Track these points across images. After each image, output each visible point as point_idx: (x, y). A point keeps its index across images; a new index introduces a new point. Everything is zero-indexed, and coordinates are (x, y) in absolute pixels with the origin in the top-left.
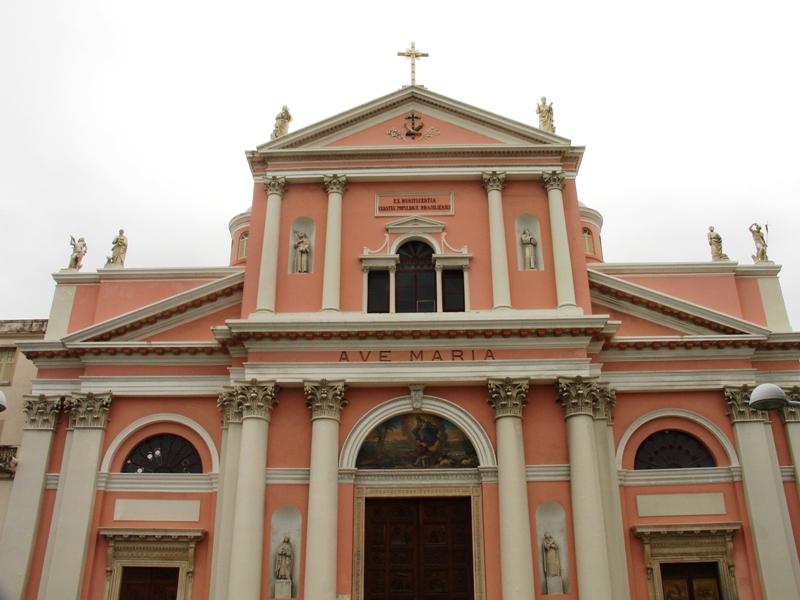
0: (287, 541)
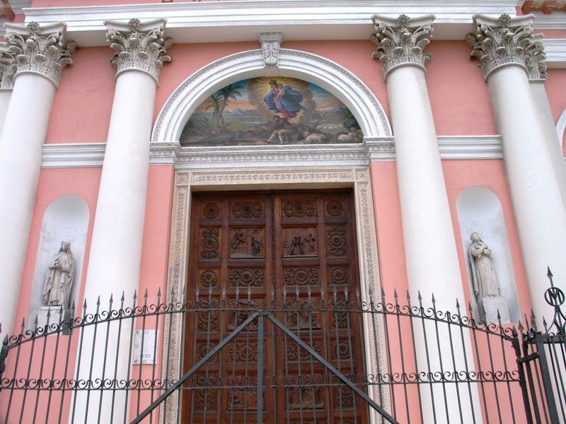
0: (66, 249)
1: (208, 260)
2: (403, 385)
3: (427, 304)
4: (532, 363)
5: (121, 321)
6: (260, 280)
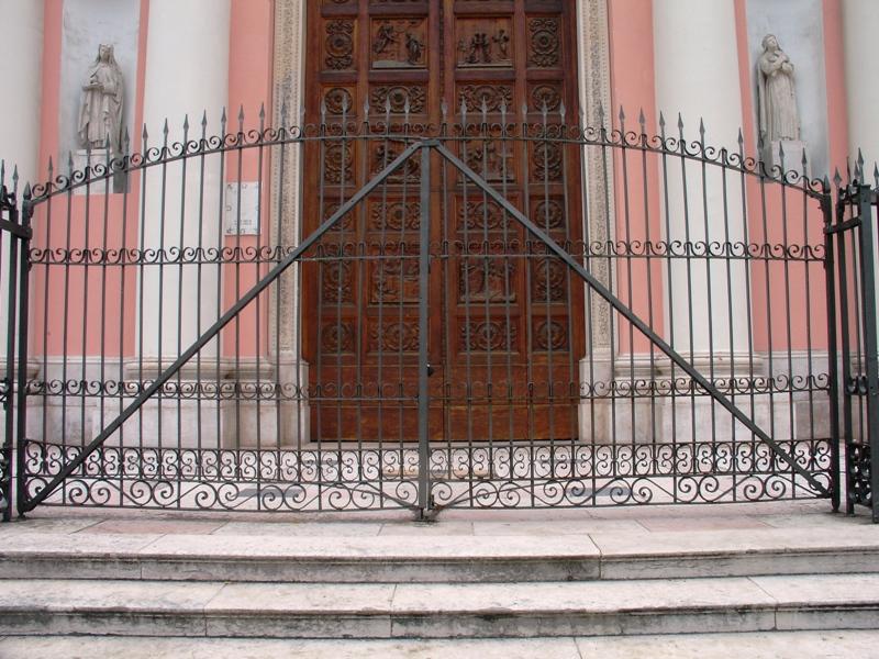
0: (106, 57)
1: (336, 71)
2: (645, 259)
3: (691, 135)
4: (847, 234)
5: (203, 158)
6: (419, 103)
